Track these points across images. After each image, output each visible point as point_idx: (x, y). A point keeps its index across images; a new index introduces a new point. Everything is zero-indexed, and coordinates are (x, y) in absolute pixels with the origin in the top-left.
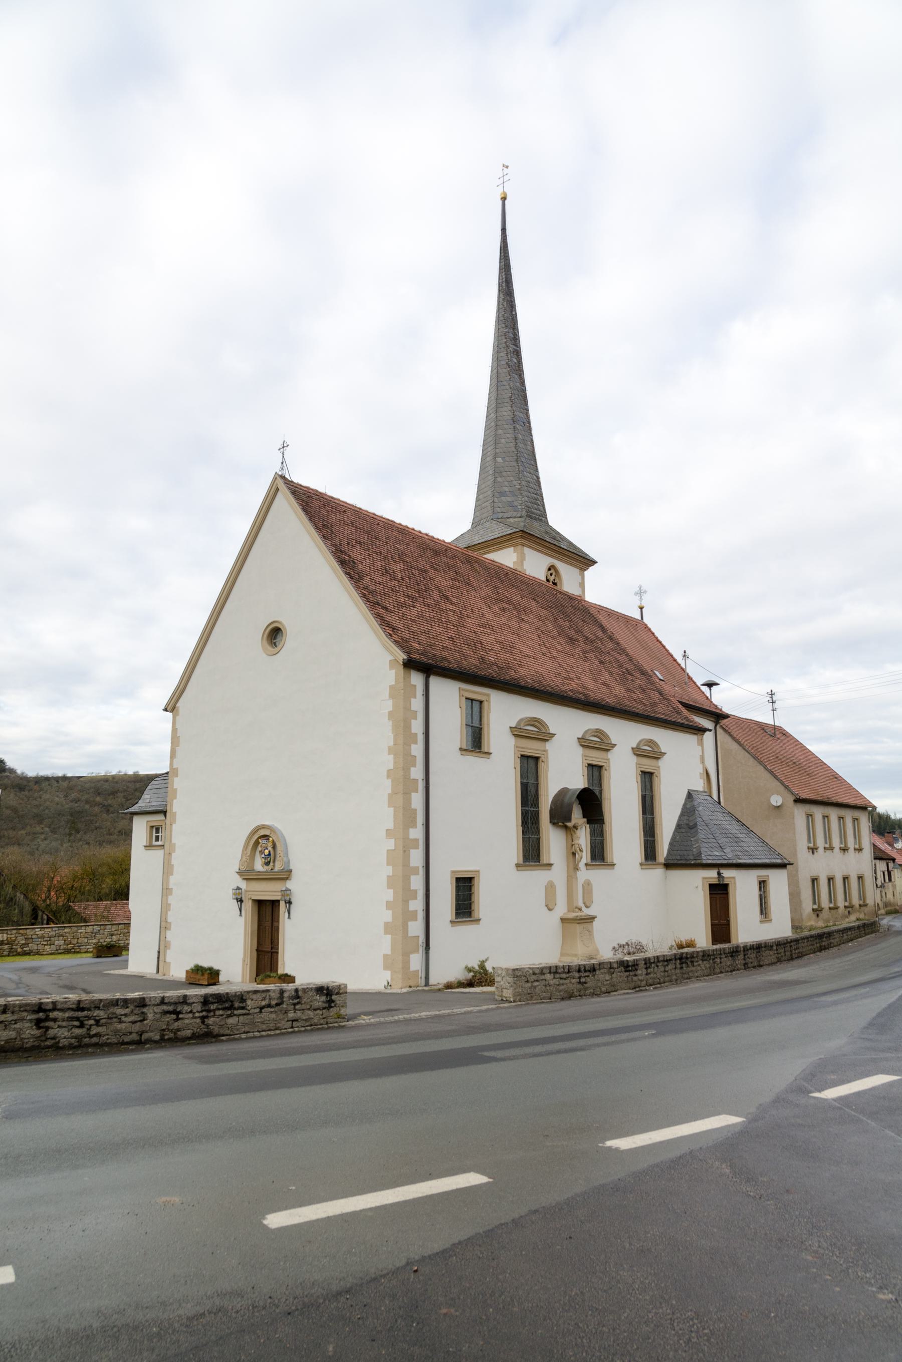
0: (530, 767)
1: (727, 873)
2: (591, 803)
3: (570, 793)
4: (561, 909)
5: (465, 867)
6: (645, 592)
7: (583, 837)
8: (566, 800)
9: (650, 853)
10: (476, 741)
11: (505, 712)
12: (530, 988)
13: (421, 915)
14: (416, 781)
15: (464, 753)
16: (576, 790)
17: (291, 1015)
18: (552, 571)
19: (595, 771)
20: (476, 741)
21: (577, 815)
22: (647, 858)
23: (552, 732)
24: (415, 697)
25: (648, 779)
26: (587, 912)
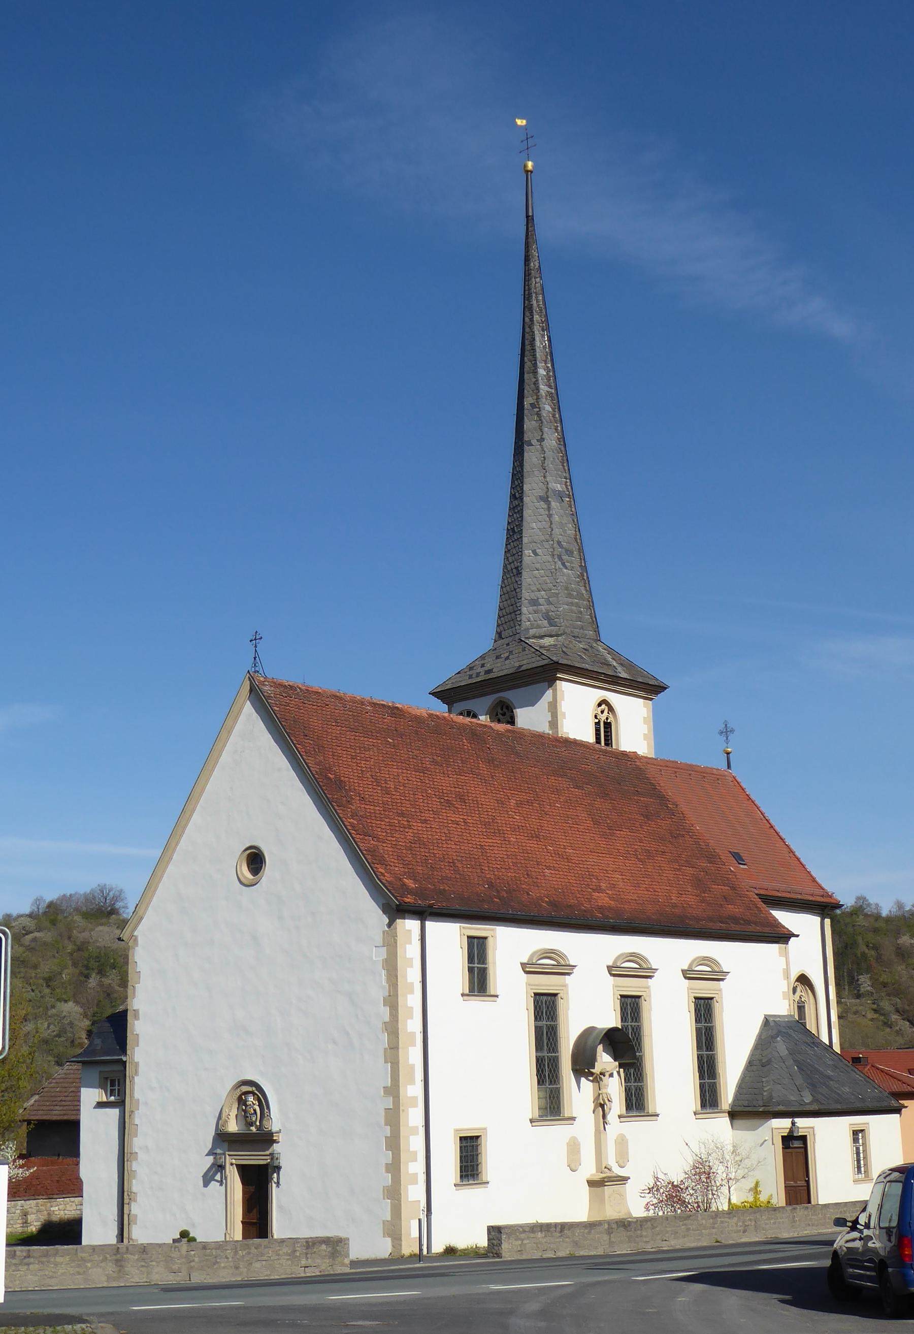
0: (546, 1008)
1: (801, 1122)
2: (624, 1044)
3: (594, 1034)
4: (589, 1170)
5: (470, 1126)
6: (732, 731)
7: (615, 1087)
8: (590, 1042)
9: (709, 1098)
10: (479, 982)
11: (511, 945)
12: (520, 1245)
13: (422, 1178)
14: (414, 1034)
15: (465, 998)
16: (603, 1029)
17: (304, 1262)
18: (603, 706)
19: (631, 1006)
20: (479, 982)
21: (605, 1060)
22: (703, 1105)
23: (572, 963)
24: (410, 943)
25: (704, 1010)
26: (618, 1171)
